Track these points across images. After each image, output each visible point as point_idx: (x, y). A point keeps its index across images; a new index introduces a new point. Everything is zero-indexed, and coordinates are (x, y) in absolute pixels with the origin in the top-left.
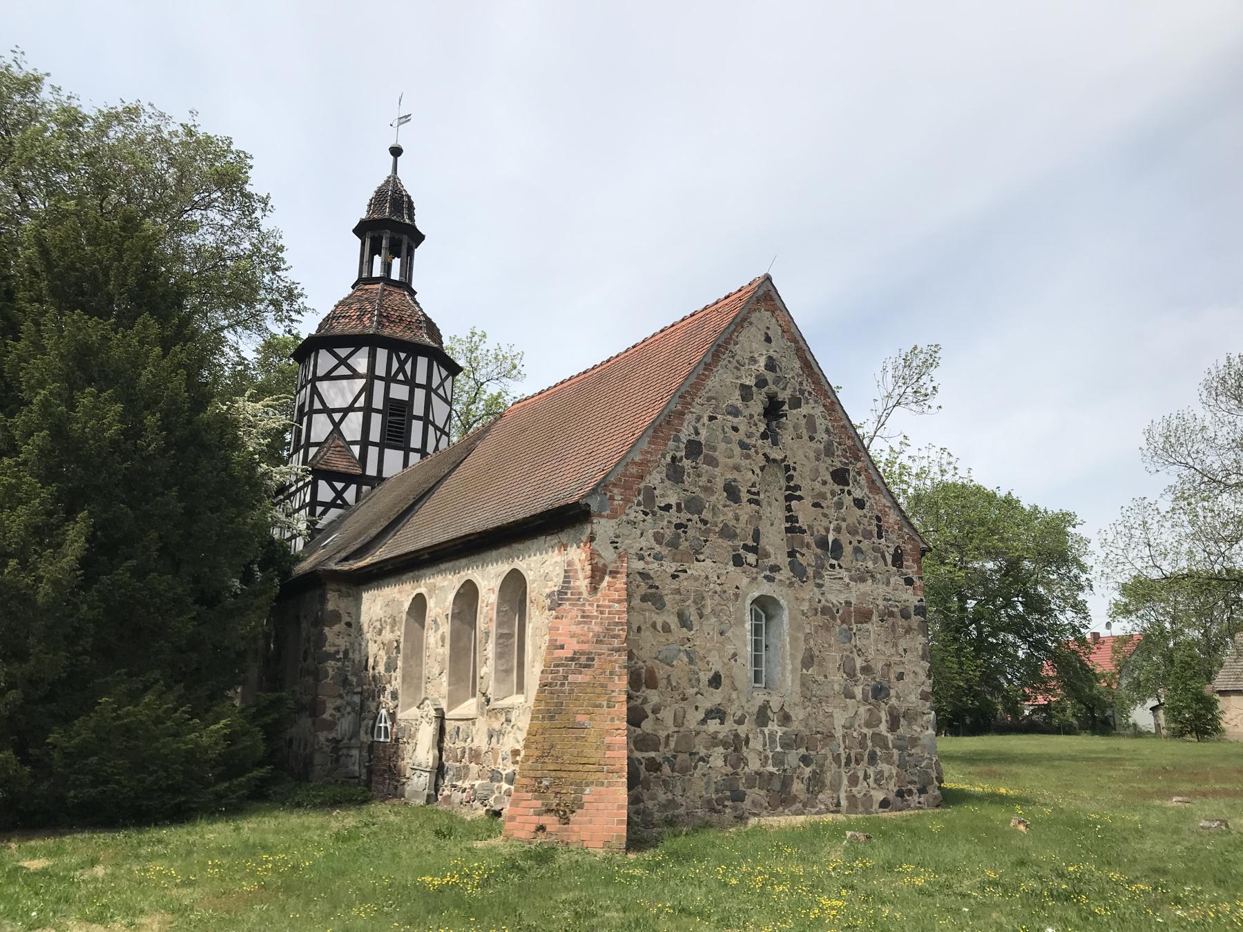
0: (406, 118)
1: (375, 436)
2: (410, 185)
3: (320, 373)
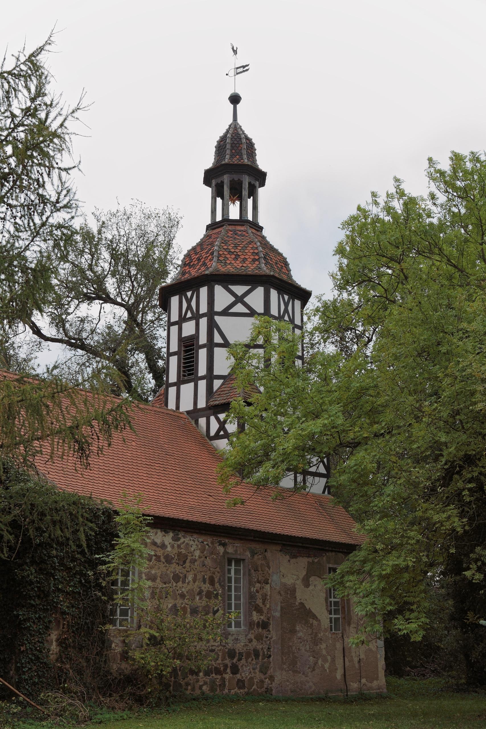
0: (244, 68)
1: (203, 354)
2: (249, 129)
3: (219, 307)
